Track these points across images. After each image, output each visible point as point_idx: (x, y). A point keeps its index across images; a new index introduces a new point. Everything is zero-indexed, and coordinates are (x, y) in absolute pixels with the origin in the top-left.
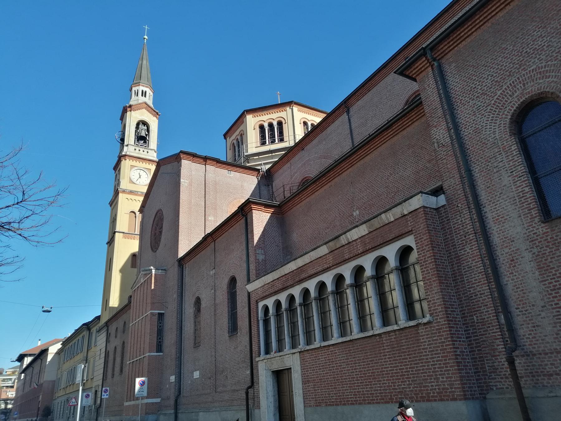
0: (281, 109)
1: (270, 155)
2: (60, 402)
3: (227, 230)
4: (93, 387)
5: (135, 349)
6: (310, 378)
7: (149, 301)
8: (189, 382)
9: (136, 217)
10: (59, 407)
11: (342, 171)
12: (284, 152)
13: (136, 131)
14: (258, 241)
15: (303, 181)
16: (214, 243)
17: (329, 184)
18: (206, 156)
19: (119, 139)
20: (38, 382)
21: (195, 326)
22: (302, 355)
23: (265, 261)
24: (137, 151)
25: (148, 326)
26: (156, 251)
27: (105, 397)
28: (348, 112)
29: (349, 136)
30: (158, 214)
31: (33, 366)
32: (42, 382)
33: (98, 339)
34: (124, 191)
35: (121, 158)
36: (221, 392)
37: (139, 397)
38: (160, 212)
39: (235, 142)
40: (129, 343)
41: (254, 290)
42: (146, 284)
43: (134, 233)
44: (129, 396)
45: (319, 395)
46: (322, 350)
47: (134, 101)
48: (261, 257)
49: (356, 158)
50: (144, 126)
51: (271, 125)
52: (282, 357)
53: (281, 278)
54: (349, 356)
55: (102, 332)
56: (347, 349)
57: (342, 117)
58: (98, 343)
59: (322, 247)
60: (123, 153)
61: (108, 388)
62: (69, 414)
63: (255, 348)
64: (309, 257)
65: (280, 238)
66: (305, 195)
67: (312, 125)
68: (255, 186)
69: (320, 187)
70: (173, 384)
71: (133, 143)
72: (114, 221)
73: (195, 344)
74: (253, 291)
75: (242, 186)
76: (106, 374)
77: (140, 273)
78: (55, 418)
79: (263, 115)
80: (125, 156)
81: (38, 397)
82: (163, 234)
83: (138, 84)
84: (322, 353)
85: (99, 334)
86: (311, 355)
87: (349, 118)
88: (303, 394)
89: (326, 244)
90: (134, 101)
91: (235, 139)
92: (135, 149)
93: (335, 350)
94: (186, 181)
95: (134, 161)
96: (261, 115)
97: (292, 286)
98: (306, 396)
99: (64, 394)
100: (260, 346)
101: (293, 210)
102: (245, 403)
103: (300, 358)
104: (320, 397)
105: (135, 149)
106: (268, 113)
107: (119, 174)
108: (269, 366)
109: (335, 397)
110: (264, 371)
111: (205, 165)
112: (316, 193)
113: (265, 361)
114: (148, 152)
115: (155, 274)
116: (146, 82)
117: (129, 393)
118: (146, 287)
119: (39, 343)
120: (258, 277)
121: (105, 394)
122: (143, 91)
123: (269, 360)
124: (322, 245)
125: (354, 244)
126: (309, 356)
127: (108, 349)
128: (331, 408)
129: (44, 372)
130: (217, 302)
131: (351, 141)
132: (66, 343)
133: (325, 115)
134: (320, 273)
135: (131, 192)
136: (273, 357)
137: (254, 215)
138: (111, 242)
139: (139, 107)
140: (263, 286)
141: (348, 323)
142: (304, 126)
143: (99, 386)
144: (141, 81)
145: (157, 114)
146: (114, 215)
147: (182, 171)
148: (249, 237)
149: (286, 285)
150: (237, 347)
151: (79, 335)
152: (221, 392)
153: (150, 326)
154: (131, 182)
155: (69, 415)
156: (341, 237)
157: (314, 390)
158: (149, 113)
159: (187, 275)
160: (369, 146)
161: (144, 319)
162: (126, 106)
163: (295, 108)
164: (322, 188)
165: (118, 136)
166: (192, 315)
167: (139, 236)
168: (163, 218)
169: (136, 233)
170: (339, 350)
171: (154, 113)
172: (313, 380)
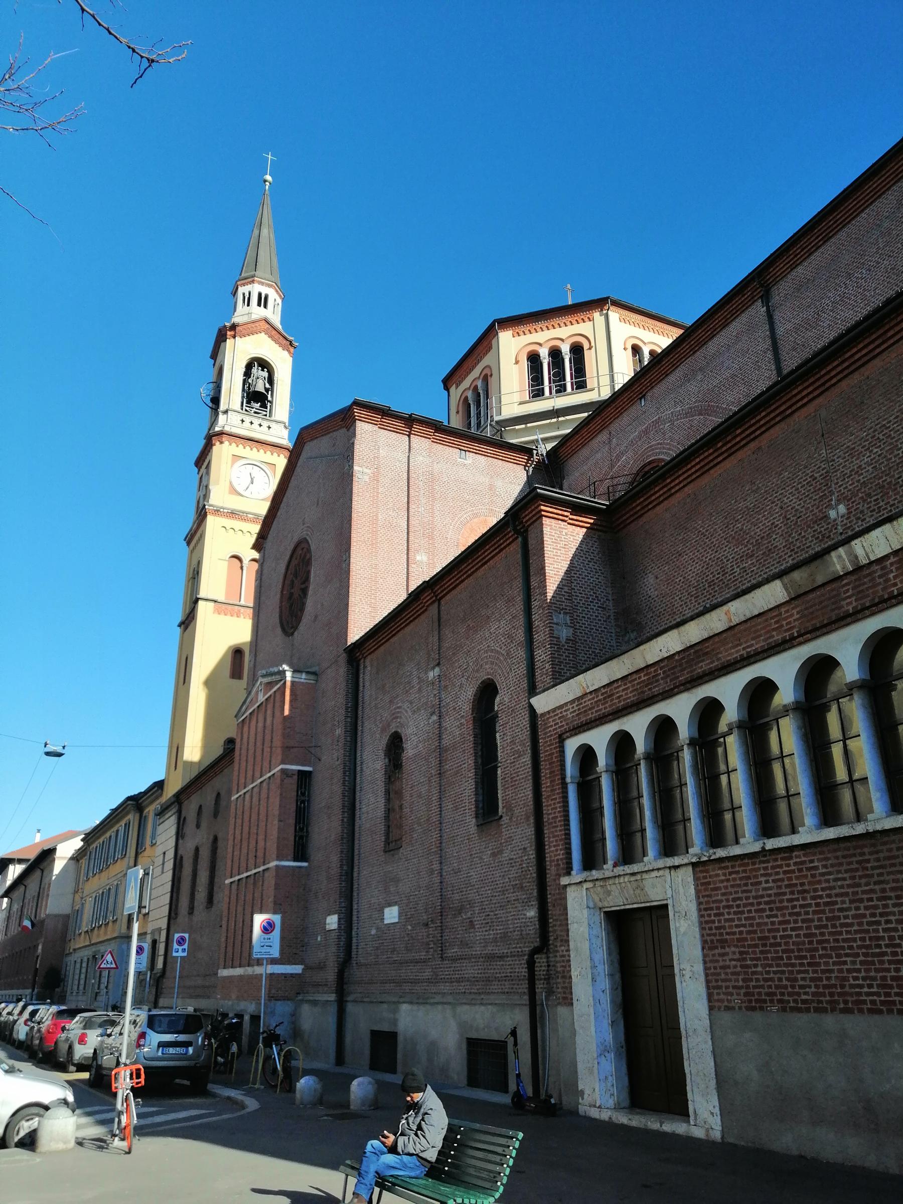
0: (581, 316)
1: (554, 420)
2: (79, 961)
3: (473, 573)
4: (149, 932)
5: (244, 851)
6: (727, 934)
7: (278, 742)
8: (373, 932)
9: (242, 568)
10: (77, 971)
11: (794, 408)
12: (586, 415)
13: (245, 382)
14: (559, 588)
15: (646, 469)
16: (436, 605)
17: (752, 445)
18: (410, 415)
19: (209, 398)
20: (35, 917)
21: (388, 800)
22: (701, 872)
23: (574, 642)
24: (247, 424)
25: (275, 802)
26: (292, 634)
27: (180, 954)
28: (766, 298)
29: (770, 355)
30: (299, 551)
31: (25, 883)
32: (43, 916)
33: (160, 829)
34: (217, 512)
35: (211, 439)
36: (454, 960)
37: (263, 959)
38: (303, 545)
39: (470, 394)
40: (231, 838)
41: (554, 710)
42: (270, 706)
43: (238, 603)
44: (230, 954)
45: (757, 980)
46: (768, 862)
47: (242, 314)
48: (565, 633)
49: (840, 368)
50: (263, 370)
51: (555, 354)
52: (638, 877)
53: (634, 676)
54: (861, 877)
55: (167, 816)
56: (854, 859)
57: (751, 311)
58: (159, 840)
59: (766, 588)
60: (217, 429)
61: (177, 936)
62: (96, 986)
63: (553, 852)
64: (724, 618)
65: (609, 590)
66: (681, 478)
67: (652, 353)
68: (521, 487)
69: (726, 455)
70: (333, 935)
71: (238, 407)
72: (195, 576)
73: (387, 842)
74: (549, 712)
75: (491, 487)
76: (177, 906)
77: (257, 680)
78: (69, 993)
79: (538, 329)
80: (221, 433)
81: (36, 947)
82: (310, 592)
83: (250, 280)
84: (765, 868)
85: (161, 820)
86: (730, 874)
87: (768, 311)
88: (707, 975)
89: (779, 576)
90: (242, 314)
91: (469, 388)
92: (243, 421)
93: (812, 861)
94: (366, 470)
95: (241, 446)
96: (533, 331)
97: (667, 695)
98: (717, 981)
99: (88, 943)
100: (570, 849)
101: (644, 519)
102: (524, 986)
103: (696, 879)
104: (762, 987)
105: (243, 421)
106: (550, 327)
107: (208, 473)
108: (597, 899)
109: (813, 989)
110: (585, 912)
111: (409, 436)
112: (712, 472)
113: (586, 885)
114: (269, 427)
115: (293, 683)
116: (268, 276)
117: (230, 949)
118: (269, 712)
119: (38, 838)
120: (559, 678)
121: (180, 948)
122: (260, 295)
123: (598, 883)
124: (768, 581)
125: (874, 572)
126: (725, 875)
127: (180, 852)
128: (802, 1020)
129: (48, 895)
130: (447, 741)
131: (773, 367)
132: (90, 837)
133: (681, 332)
134: (758, 658)
135: (233, 514)
136: (611, 874)
137: (546, 530)
138: (188, 621)
139: (251, 328)
140: (578, 699)
141: (680, 827)
142: (634, 355)
143: (160, 930)
144: (257, 273)
145: (291, 344)
146: (195, 562)
147: (357, 447)
148: (534, 583)
149: (648, 693)
150: (501, 852)
151: (118, 821)
152: (454, 960)
153: (281, 801)
154: (234, 491)
155: (99, 988)
156: (833, 554)
157: (742, 966)
158: (273, 343)
159: (367, 684)
160: (881, 331)
161: (265, 784)
162: (225, 326)
163: (614, 315)
164: (732, 457)
165: (205, 391)
166: (380, 776)
167: (251, 610)
168: (310, 559)
169: (243, 602)
170: (827, 859)
171: (285, 342)
172: (738, 940)
